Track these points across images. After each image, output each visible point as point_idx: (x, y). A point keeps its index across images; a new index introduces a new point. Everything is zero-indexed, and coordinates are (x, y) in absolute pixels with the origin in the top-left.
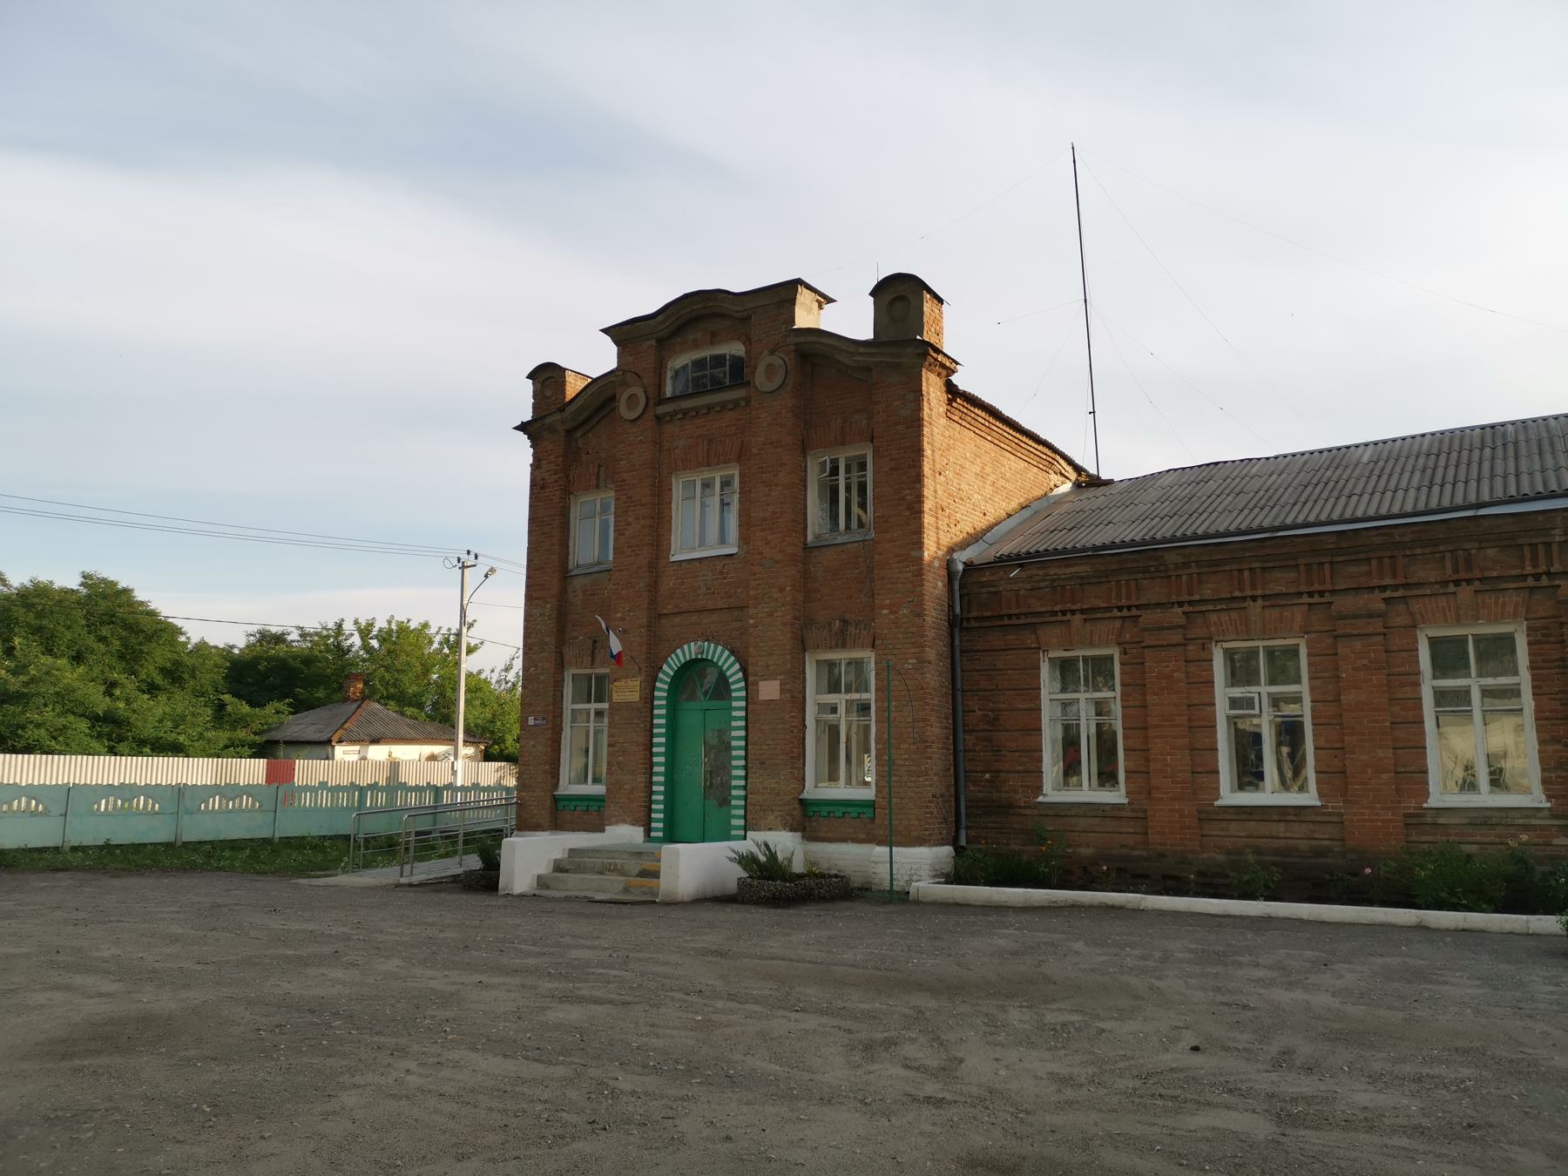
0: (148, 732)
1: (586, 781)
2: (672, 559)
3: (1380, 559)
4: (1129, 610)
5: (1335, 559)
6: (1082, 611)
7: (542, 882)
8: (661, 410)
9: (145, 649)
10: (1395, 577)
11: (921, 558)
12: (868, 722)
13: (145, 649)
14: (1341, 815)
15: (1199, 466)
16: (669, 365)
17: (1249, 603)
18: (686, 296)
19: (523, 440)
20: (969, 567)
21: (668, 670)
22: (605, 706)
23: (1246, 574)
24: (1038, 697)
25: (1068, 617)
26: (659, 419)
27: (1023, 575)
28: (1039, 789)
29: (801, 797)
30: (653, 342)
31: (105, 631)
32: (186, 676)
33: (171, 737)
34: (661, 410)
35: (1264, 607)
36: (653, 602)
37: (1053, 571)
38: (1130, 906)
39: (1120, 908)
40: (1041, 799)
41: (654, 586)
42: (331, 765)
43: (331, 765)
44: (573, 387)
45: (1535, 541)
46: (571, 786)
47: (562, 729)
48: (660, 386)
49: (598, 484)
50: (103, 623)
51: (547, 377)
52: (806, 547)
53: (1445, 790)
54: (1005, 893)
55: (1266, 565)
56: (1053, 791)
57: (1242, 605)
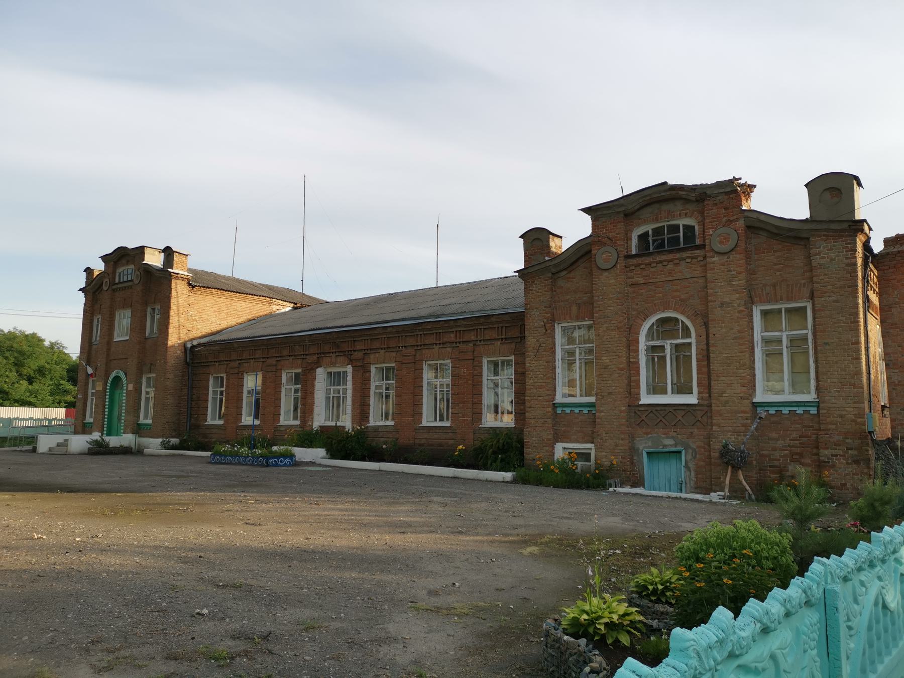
0: (17, 397)
1: (436, 419)
2: (115, 340)
3: (318, 344)
4: (421, 347)
5: (269, 347)
6: (219, 361)
7: (50, 449)
8: (114, 287)
9: (25, 361)
10: (348, 348)
11: (167, 344)
12: (248, 395)
13: (25, 361)
14: (263, 427)
15: (432, 288)
16: (117, 271)
17: (331, 354)
18: (119, 248)
19: (82, 296)
20: (193, 347)
21: (110, 379)
22: (94, 391)
23: (383, 339)
24: (208, 390)
25: (458, 345)
26: (114, 290)
27: (205, 349)
28: (206, 420)
29: (139, 423)
30: (113, 263)
31: (7, 354)
32: (47, 373)
33: (28, 399)
34: (114, 287)
35: (336, 356)
36: (108, 355)
37: (211, 348)
38: (184, 454)
39: (182, 455)
40: (206, 423)
41: (109, 350)
42: (9, 414)
43: (9, 414)
44: (96, 273)
45: (481, 327)
46: (326, 422)
47: (88, 399)
48: (114, 278)
49: (633, 213)
50: (8, 351)
51: (88, 271)
52: (146, 338)
53: (213, 419)
54: (470, 472)
55: (256, 348)
56: (210, 421)
57: (248, 361)
